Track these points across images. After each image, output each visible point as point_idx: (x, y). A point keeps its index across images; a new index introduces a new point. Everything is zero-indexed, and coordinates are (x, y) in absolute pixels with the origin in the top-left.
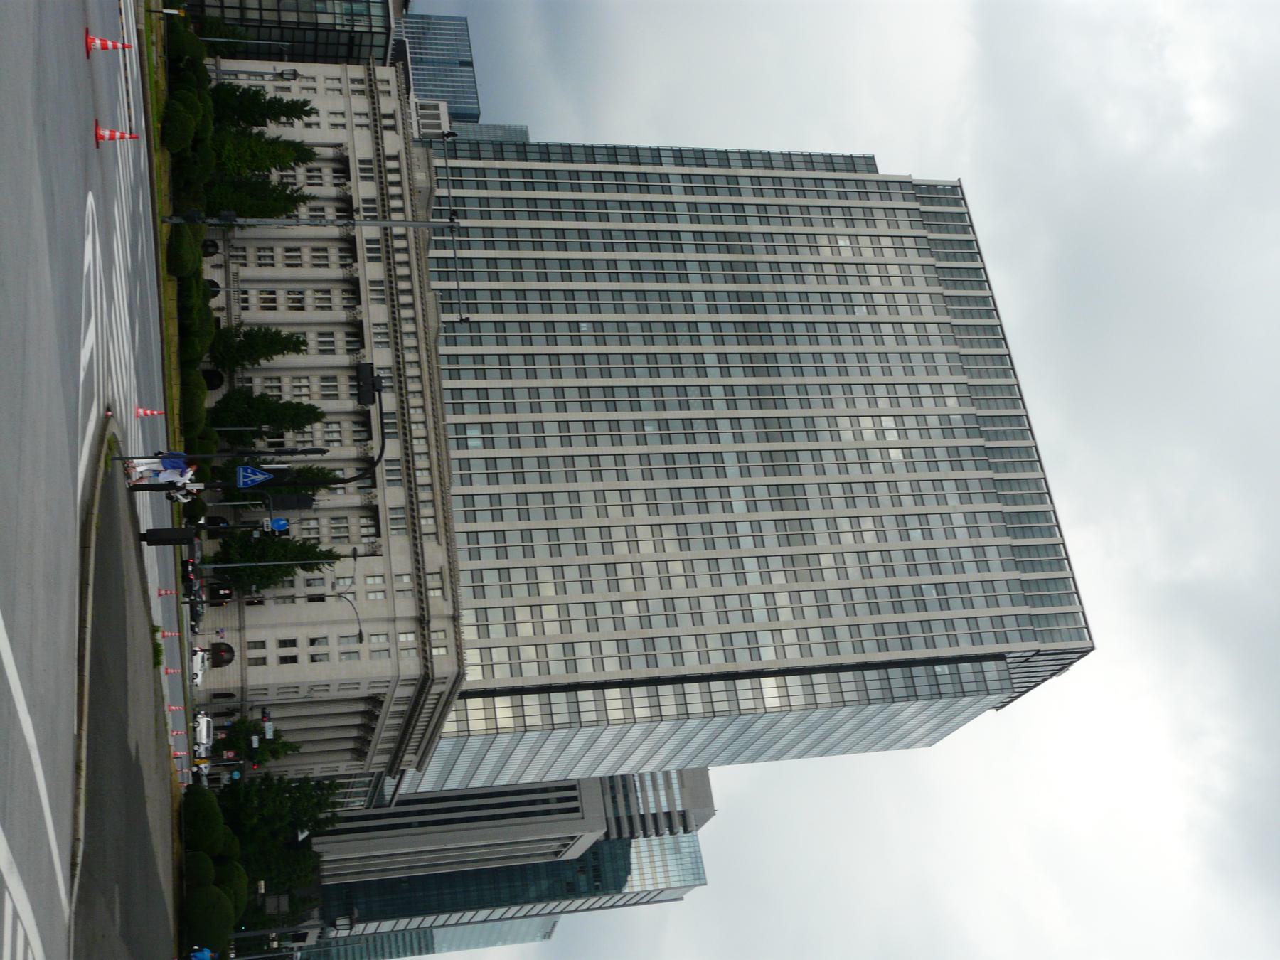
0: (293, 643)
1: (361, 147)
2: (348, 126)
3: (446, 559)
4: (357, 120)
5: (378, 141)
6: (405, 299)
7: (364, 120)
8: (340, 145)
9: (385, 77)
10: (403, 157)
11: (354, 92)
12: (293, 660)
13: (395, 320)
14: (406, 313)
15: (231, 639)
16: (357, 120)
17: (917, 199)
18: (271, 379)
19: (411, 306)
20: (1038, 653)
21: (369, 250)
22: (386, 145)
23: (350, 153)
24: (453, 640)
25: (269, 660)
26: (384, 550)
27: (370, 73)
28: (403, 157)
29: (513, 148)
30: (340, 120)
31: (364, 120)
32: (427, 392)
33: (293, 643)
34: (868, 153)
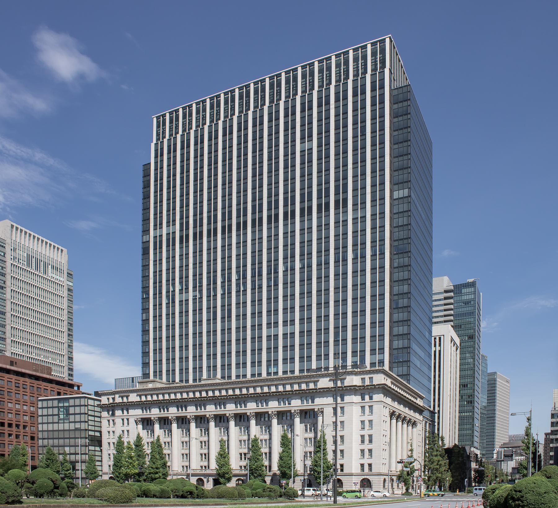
0: (371, 441)
2: (342, 405)
15: (358, 480)
20: (391, 72)
34: (141, 168)
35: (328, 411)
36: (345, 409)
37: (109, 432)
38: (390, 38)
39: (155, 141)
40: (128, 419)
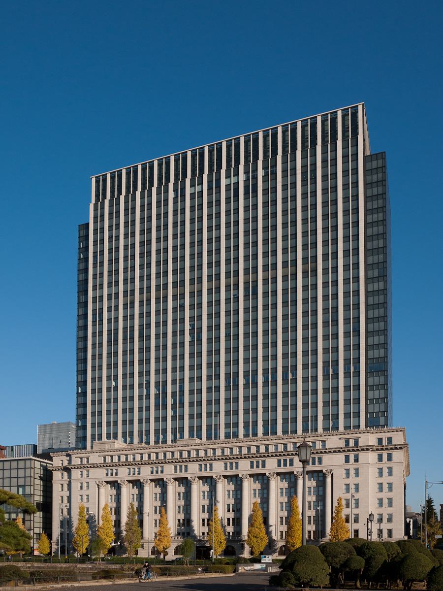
2: (356, 467)
5: (94, 466)
7: (85, 473)
11: (356, 460)
21: (181, 471)
31: (85, 473)
35: (339, 473)
36: (360, 471)
37: (390, 520)
38: (363, 104)
39: (93, 201)
40: (88, 483)
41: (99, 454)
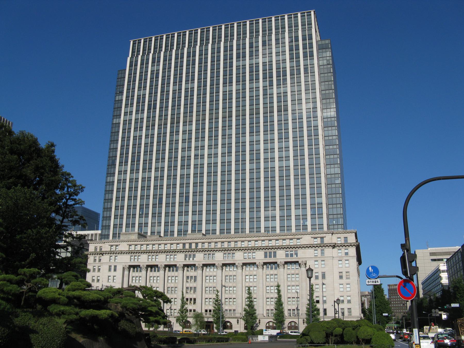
0: (115, 270)
1: (125, 260)
2: (115, 265)
3: (125, 243)
4: (112, 261)
6: (193, 246)
8: (124, 268)
9: (94, 248)
10: (130, 243)
12: (110, 270)
13: (203, 250)
14: (200, 246)
16: (112, 261)
17: (137, 56)
18: (168, 291)
19: (197, 244)
22: (125, 250)
23: (127, 265)
24: (342, 234)
25: (110, 273)
26: (304, 260)
27: (92, 254)
28: (130, 243)
29: (106, 204)
30: (113, 268)
32: (236, 239)
33: (115, 270)
41: (127, 243)
